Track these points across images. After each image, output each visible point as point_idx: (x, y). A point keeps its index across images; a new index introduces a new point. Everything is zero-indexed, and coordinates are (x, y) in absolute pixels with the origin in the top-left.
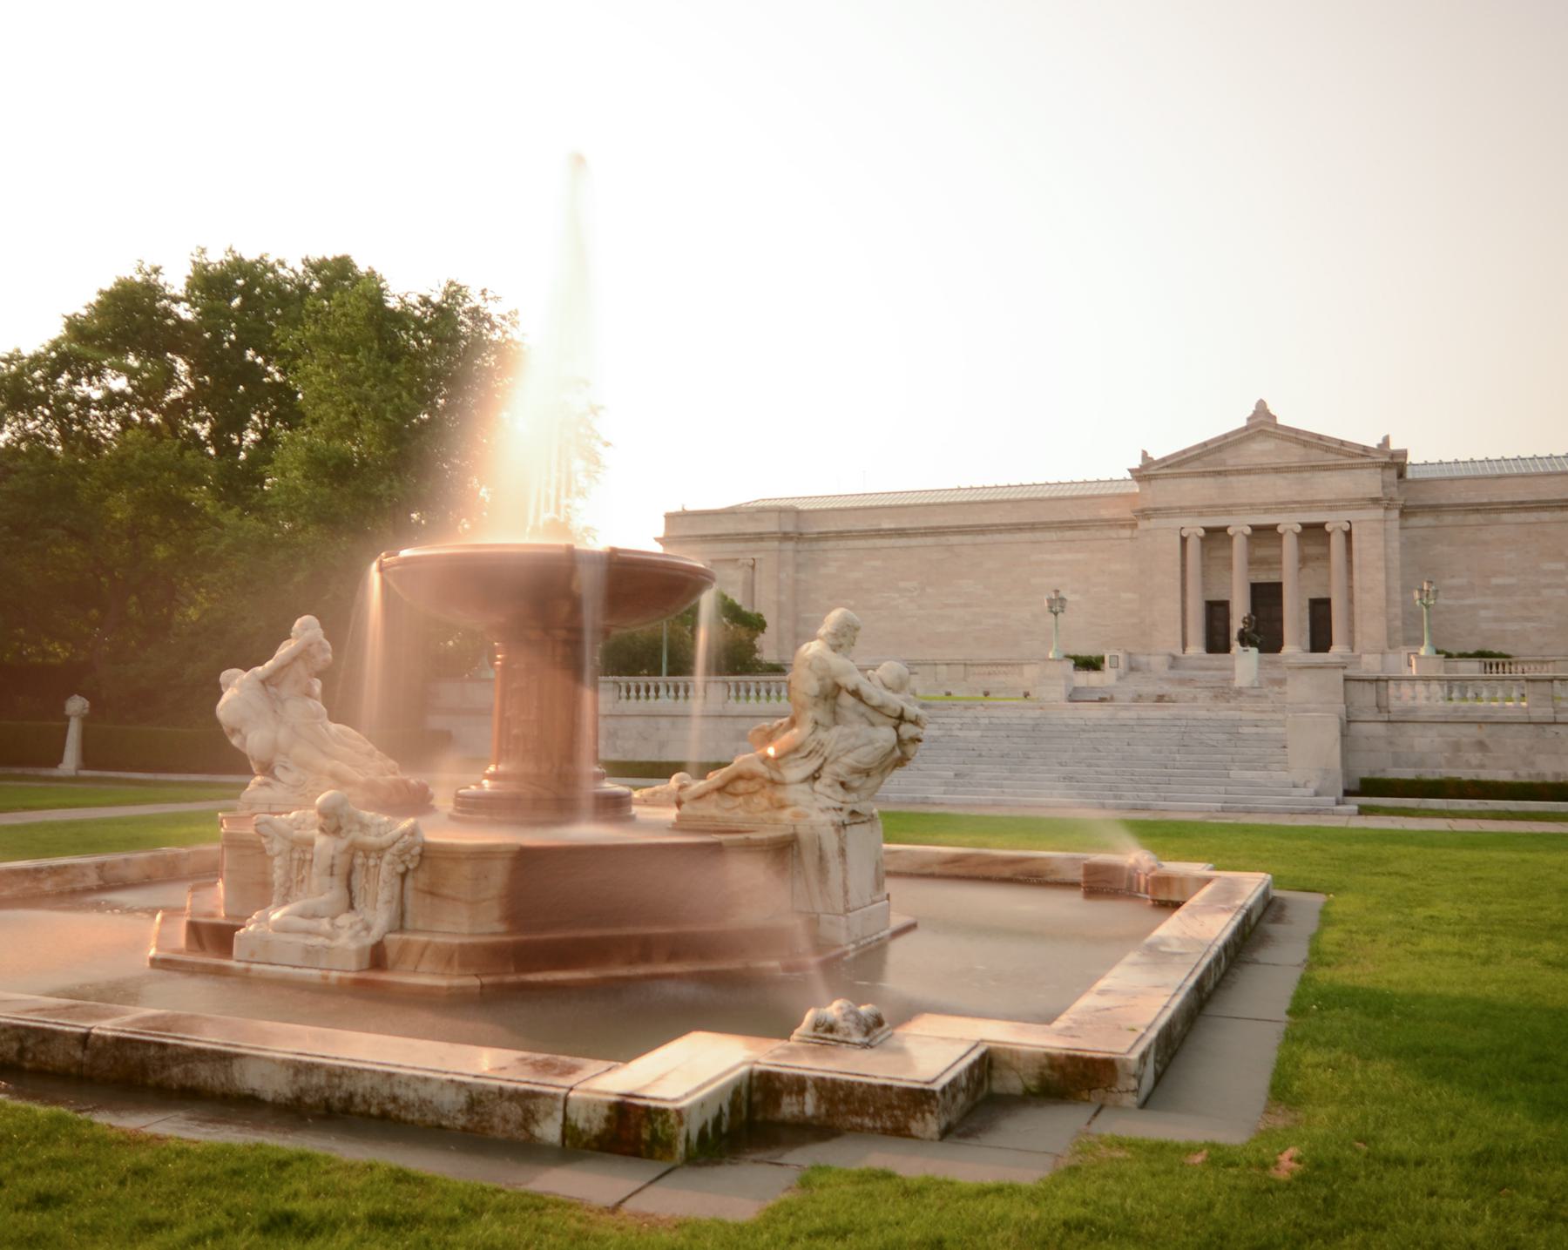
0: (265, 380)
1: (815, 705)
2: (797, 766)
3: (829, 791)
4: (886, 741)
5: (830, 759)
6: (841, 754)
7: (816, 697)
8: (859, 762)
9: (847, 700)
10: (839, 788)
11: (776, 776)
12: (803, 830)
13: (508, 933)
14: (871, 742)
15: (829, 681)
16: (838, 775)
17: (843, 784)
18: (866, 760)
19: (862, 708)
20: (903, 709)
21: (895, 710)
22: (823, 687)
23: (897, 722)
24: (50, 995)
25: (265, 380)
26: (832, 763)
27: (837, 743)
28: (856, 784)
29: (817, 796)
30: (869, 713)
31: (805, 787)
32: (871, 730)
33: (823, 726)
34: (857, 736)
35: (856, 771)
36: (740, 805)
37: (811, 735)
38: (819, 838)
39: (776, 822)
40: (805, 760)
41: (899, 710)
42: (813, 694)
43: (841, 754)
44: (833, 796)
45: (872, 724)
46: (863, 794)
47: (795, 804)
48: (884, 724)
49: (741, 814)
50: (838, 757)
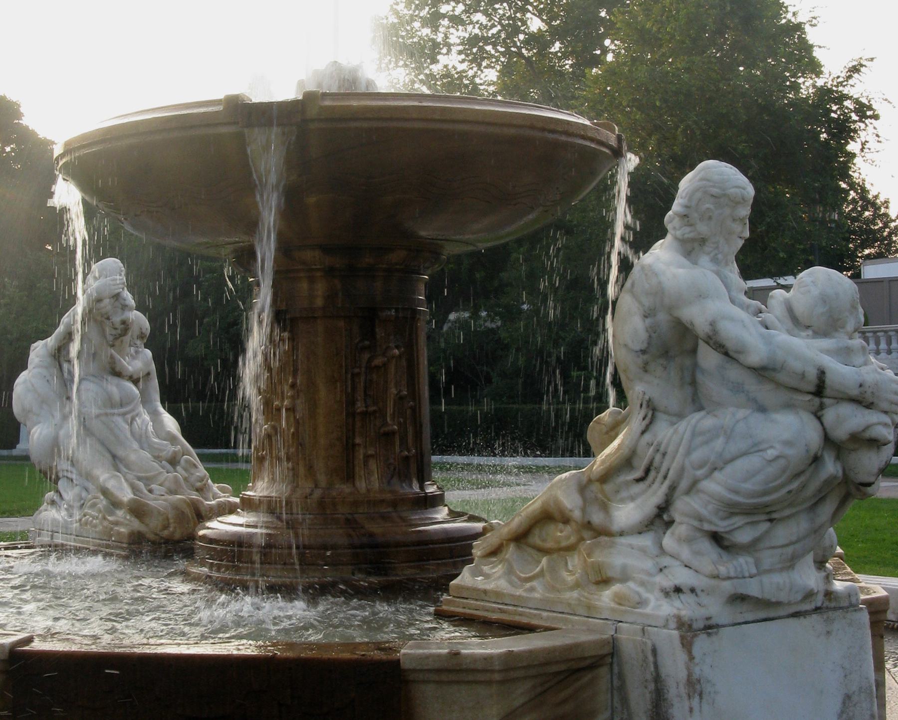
0: (223, 569)
1: (645, 368)
2: (632, 499)
3: (685, 553)
4: (788, 443)
5: (684, 485)
6: (700, 473)
7: (643, 352)
8: (736, 492)
9: (708, 358)
10: (706, 545)
11: (597, 518)
12: (628, 635)
13: (263, 479)
14: (756, 448)
15: (662, 317)
16: (701, 519)
17: (716, 538)
18: (748, 486)
19: (734, 373)
20: (822, 373)
21: (803, 376)
22: (652, 330)
23: (817, 400)
24: (753, 497)
25: (223, 569)
26: (688, 492)
27: (688, 453)
28: (744, 537)
29: (666, 561)
30: (751, 384)
31: (646, 541)
32: (756, 419)
33: (666, 413)
34: (729, 433)
35: (732, 509)
36: (541, 574)
37: (643, 432)
38: (654, 651)
39: (590, 610)
40: (642, 486)
41: (812, 374)
42: (638, 347)
43: (700, 473)
44: (695, 563)
45: (762, 409)
46: (768, 558)
47: (624, 578)
48: (789, 406)
49: (539, 591)
50: (695, 483)
